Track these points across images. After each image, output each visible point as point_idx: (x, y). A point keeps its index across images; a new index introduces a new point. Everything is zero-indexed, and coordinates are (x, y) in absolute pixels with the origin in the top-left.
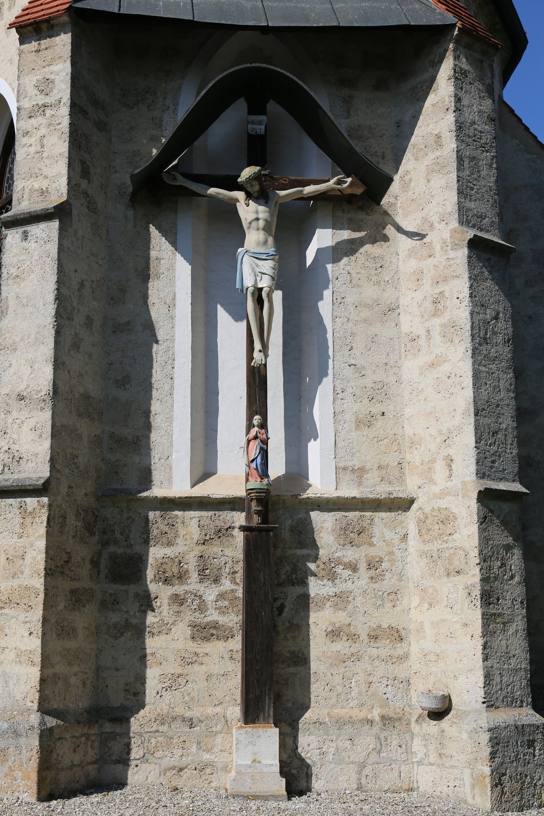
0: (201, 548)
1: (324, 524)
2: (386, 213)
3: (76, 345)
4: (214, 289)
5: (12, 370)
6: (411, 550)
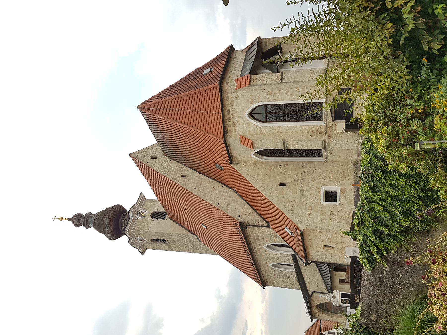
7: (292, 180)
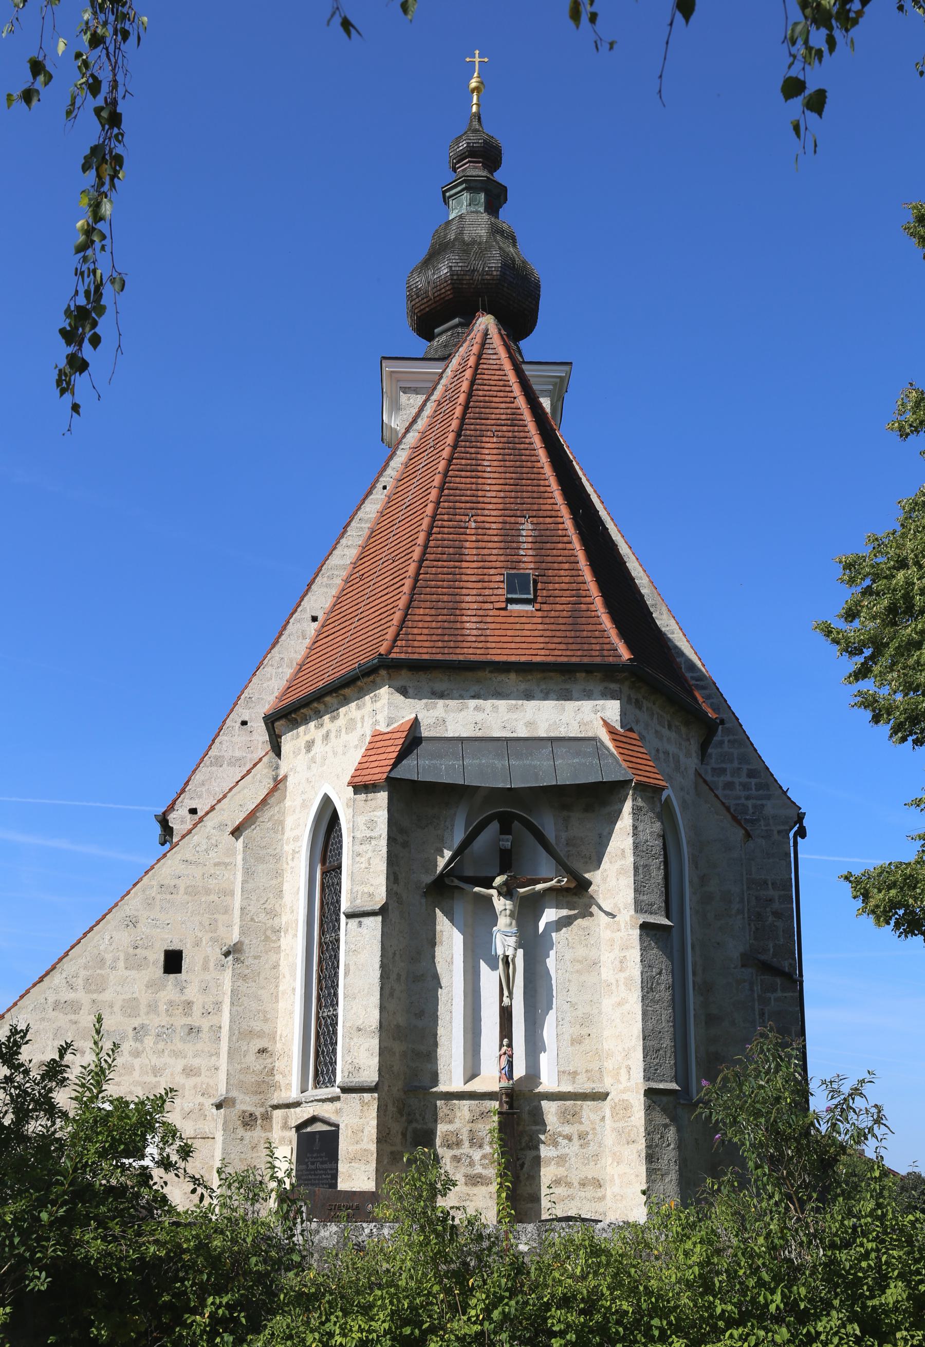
0: (471, 1125)
1: (550, 1109)
2: (592, 897)
3: (391, 995)
4: (478, 950)
5: (353, 1011)
6: (607, 1127)
7: (192, 992)
